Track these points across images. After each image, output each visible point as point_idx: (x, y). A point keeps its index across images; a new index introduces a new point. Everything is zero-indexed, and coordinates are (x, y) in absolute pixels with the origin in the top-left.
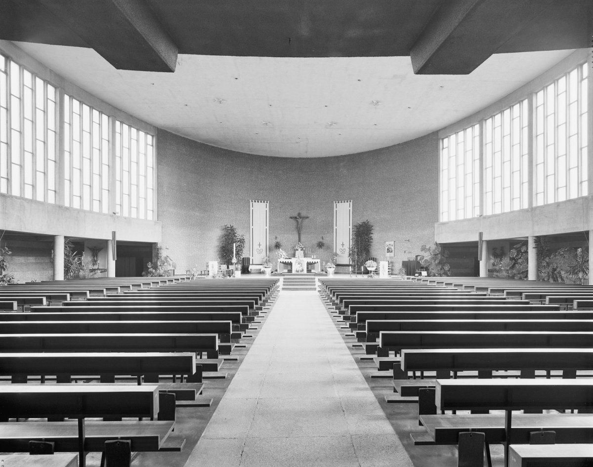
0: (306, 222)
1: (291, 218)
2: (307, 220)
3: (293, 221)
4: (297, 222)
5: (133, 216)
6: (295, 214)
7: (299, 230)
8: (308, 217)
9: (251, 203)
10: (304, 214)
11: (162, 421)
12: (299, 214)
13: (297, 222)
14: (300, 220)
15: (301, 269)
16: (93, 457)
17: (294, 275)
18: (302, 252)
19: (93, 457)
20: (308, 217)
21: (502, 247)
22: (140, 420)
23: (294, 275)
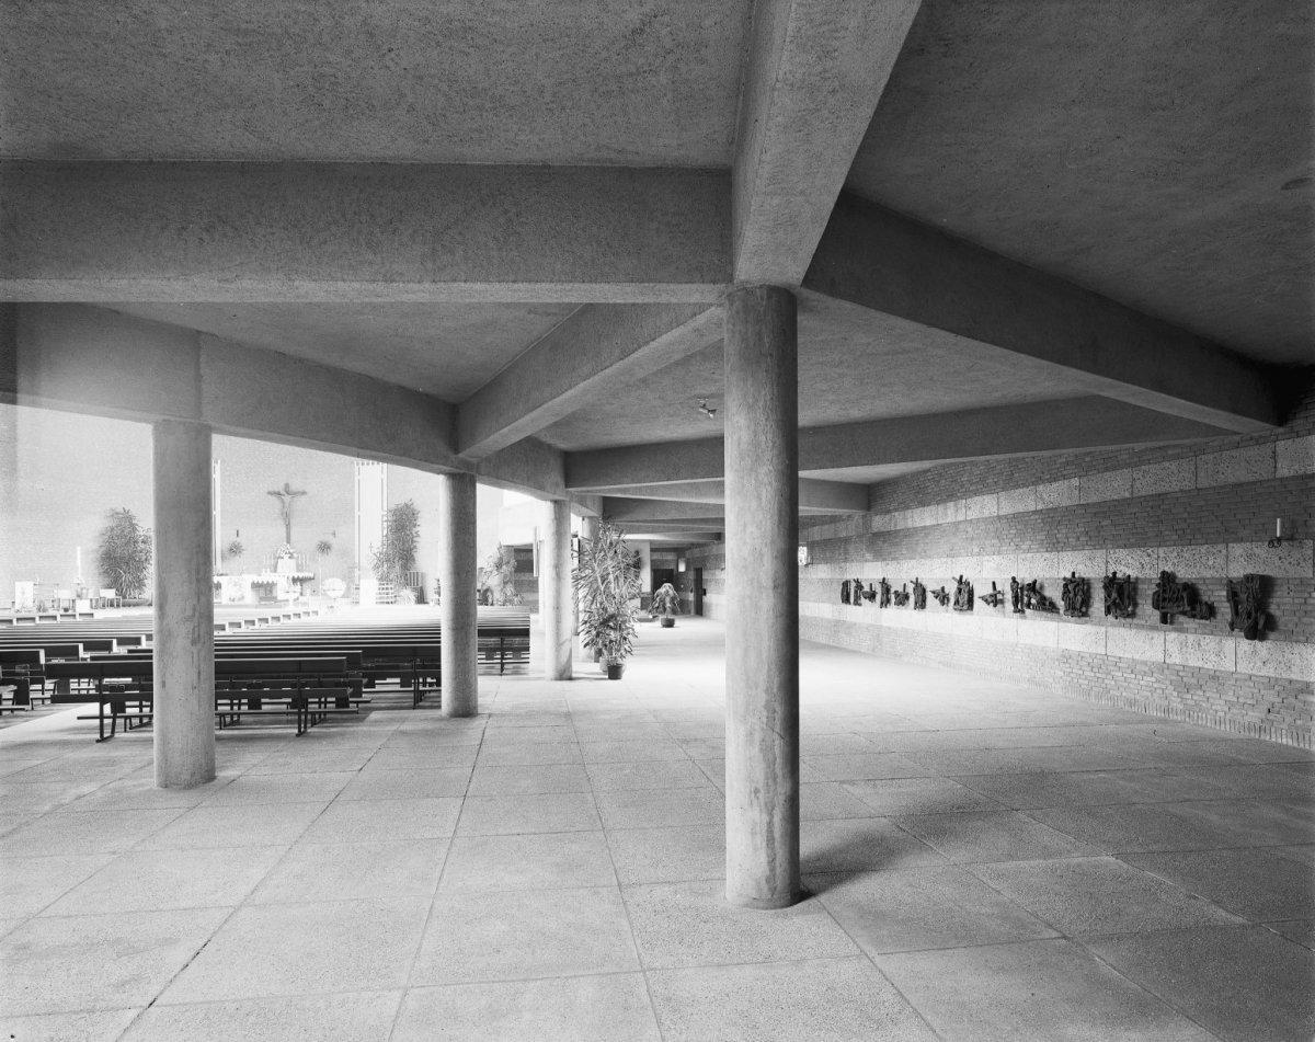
0: (301, 502)
1: (269, 493)
2: (303, 498)
3: (274, 499)
4: (283, 502)
5: (310, 706)
6: (280, 488)
7: (287, 518)
8: (304, 493)
9: (357, 467)
10: (296, 486)
11: (910, 464)
12: (287, 485)
13: (283, 502)
14: (287, 498)
15: (238, 595)
16: (762, 555)
17: (226, 606)
18: (293, 562)
19: (762, 555)
20: (304, 493)
21: (637, 552)
22: (669, 624)
23: (226, 606)
